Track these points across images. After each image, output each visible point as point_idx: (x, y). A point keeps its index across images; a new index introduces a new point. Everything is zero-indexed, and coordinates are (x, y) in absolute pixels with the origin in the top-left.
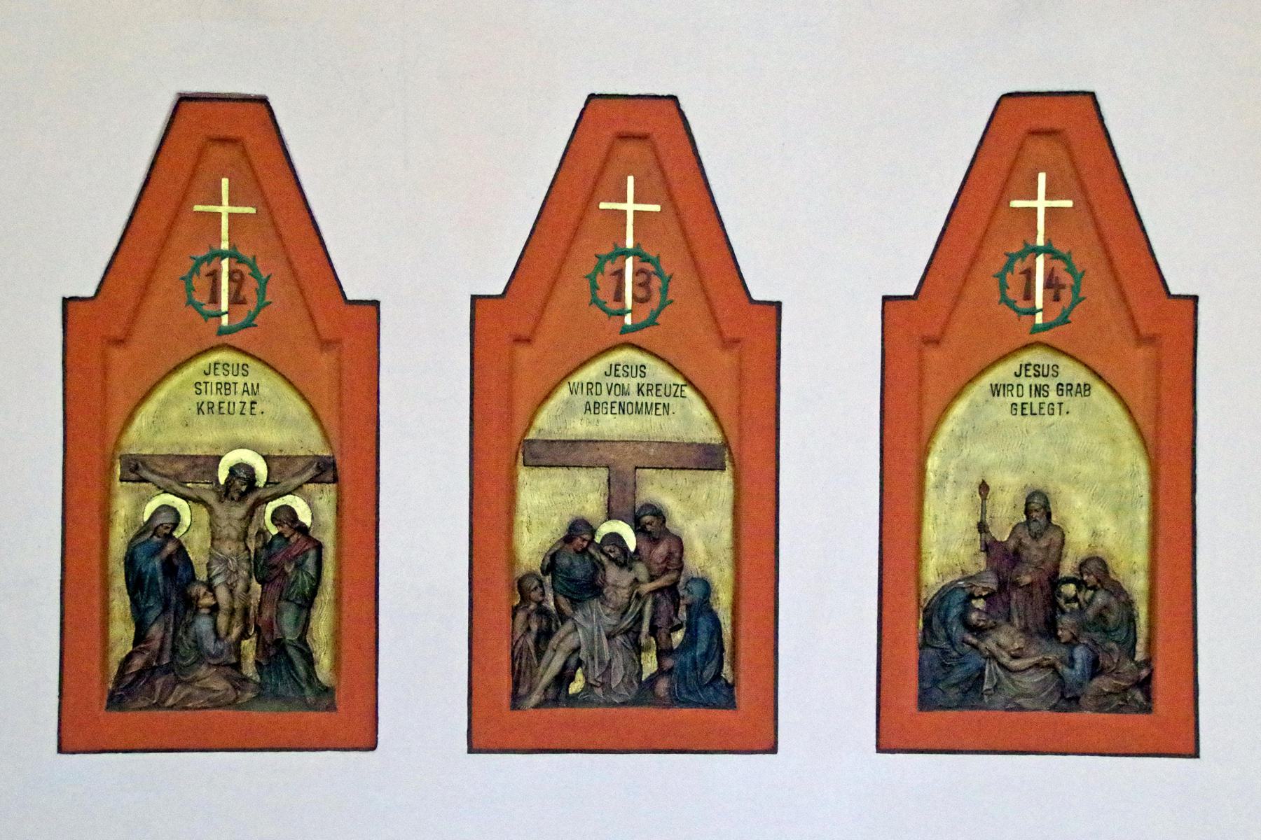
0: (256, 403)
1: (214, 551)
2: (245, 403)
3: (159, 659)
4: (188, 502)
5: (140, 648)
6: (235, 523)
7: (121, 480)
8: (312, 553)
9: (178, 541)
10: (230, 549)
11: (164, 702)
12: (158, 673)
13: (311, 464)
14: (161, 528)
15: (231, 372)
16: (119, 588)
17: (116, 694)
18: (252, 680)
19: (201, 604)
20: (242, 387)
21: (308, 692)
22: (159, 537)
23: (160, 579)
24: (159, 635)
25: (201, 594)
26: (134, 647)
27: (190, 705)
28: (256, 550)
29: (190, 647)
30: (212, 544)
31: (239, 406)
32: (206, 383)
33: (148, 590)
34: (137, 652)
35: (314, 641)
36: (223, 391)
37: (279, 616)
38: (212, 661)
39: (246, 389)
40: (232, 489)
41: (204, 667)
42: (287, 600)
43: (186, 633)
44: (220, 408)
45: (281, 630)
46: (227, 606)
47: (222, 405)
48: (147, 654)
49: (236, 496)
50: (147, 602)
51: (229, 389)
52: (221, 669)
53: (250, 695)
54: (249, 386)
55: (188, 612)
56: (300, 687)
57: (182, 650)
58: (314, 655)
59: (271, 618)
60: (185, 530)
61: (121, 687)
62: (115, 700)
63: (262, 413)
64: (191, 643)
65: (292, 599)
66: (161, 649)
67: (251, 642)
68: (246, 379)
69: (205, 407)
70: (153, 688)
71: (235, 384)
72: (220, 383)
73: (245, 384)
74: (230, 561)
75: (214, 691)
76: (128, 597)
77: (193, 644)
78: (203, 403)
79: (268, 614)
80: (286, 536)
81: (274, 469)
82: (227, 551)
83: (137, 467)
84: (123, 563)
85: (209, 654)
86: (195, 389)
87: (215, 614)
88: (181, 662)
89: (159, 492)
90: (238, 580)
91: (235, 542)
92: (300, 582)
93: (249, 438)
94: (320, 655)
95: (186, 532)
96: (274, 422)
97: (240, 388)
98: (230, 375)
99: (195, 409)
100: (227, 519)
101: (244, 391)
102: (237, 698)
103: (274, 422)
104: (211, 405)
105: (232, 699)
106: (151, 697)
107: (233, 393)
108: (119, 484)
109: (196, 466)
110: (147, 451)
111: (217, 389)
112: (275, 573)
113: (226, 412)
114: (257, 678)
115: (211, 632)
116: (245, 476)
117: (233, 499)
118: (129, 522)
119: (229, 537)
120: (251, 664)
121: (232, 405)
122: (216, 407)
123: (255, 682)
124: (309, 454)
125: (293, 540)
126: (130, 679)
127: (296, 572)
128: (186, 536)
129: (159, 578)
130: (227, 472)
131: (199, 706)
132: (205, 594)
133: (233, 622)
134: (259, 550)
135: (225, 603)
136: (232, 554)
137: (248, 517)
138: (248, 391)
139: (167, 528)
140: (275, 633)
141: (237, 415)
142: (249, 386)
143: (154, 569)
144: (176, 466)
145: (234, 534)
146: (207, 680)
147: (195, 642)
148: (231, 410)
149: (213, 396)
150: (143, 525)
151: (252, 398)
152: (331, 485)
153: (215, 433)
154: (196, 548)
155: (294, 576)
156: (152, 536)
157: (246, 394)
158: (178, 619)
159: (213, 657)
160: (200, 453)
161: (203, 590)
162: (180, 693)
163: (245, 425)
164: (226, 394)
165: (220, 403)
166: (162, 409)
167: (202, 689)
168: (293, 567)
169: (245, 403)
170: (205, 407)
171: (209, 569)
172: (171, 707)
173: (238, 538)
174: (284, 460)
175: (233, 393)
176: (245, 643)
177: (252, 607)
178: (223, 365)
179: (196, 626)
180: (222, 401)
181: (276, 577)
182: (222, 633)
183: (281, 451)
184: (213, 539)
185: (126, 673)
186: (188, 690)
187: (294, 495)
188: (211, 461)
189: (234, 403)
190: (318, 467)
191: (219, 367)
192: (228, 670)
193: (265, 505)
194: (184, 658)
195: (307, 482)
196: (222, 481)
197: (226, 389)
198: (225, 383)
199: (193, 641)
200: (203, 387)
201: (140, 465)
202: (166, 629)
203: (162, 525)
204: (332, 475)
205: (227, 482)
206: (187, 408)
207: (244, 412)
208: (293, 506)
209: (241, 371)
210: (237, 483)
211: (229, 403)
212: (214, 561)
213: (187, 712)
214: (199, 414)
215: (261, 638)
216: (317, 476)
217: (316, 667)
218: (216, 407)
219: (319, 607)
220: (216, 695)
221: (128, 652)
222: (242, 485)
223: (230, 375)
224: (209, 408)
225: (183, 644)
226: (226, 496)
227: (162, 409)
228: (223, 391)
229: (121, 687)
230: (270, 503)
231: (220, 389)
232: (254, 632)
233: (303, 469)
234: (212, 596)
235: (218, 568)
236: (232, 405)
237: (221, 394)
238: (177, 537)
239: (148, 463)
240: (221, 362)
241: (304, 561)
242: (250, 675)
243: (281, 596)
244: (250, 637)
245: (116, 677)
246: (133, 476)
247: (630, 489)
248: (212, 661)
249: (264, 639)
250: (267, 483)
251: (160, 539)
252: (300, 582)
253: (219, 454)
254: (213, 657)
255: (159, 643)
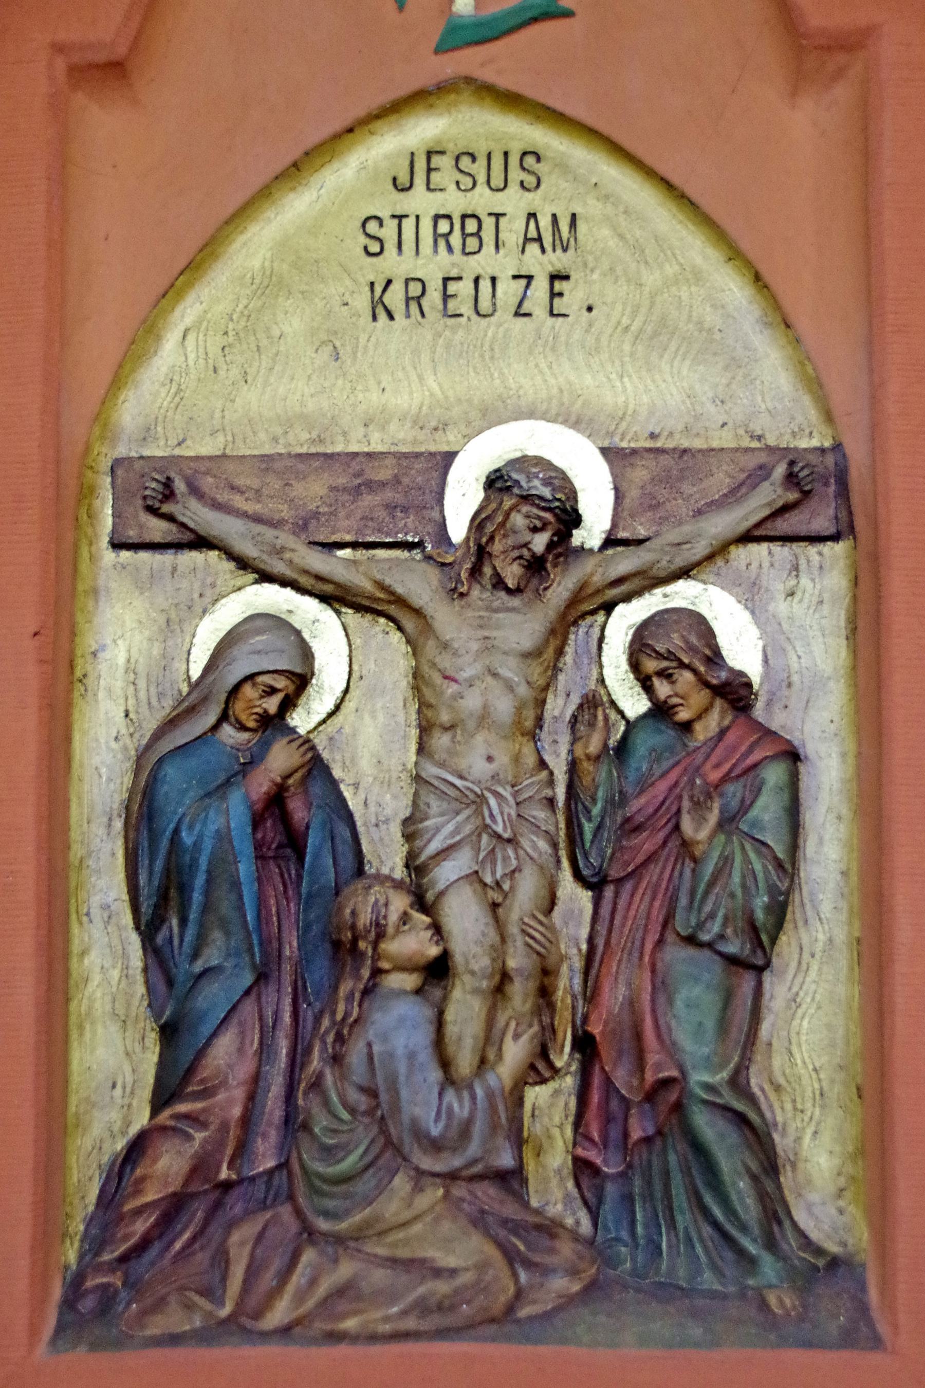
0: (567, 278)
1: (431, 770)
2: (530, 278)
3: (242, 1149)
4: (338, 613)
5: (178, 1117)
6: (510, 669)
7: (117, 545)
8: (774, 774)
9: (307, 742)
10: (490, 759)
11: (258, 1315)
12: (235, 1205)
13: (762, 473)
14: (248, 691)
15: (481, 178)
16: (105, 907)
17: (89, 1284)
18: (563, 1227)
19: (389, 958)
20: (520, 224)
21: (769, 1267)
22: (243, 728)
23: (245, 869)
24: (244, 1070)
25: (393, 917)
26: (155, 1112)
27: (350, 1324)
28: (573, 767)
29: (352, 1111)
30: (421, 749)
31: (509, 290)
32: (400, 218)
33: (206, 908)
34: (163, 1129)
35: (778, 1088)
36: (456, 240)
37: (661, 999)
38: (427, 1163)
39: (532, 233)
40: (497, 547)
41: (401, 1183)
42: (691, 940)
43: (337, 1060)
44: (446, 297)
45: (670, 1049)
46: (482, 963)
47: (452, 287)
48: (199, 1136)
49: (512, 573)
50: (195, 955)
51: (477, 235)
52: (459, 1190)
53: (560, 1284)
54: (545, 222)
55: (345, 988)
56: (741, 1252)
57: (321, 1122)
58: (776, 1137)
59: (632, 1003)
60: (329, 706)
61: (106, 1257)
62: (87, 1304)
63: (590, 309)
64: (354, 1096)
65: (705, 937)
66: (247, 1121)
67: (557, 1093)
68: (533, 200)
69: (395, 298)
70: (222, 1260)
71: (498, 216)
72: (448, 217)
73: (532, 216)
74: (493, 802)
75: (438, 1273)
76: (135, 940)
77: (362, 1102)
78: (389, 282)
79: (622, 991)
80: (683, 715)
81: (633, 494)
82: (479, 767)
83: (168, 493)
84: (119, 824)
85: (419, 1134)
86: (363, 240)
87: (438, 993)
88: (318, 1167)
89: (239, 582)
90: (518, 869)
91: (505, 738)
92: (736, 878)
93: (543, 394)
94: (798, 1140)
95: (331, 715)
96: (629, 337)
97: (513, 231)
98: (482, 188)
99: (362, 302)
100: (479, 653)
101: (527, 240)
102: (519, 1294)
103: (629, 337)
104: (415, 289)
105: (503, 1299)
106: (211, 1293)
107: (489, 246)
108: (109, 556)
109: (371, 486)
110: (207, 447)
111: (436, 236)
112: (646, 843)
113: (466, 309)
114: (578, 1223)
115: (426, 1056)
116: (546, 492)
117: (499, 583)
118: (142, 684)
119: (484, 718)
120: (559, 1171)
121: (485, 285)
122: (434, 296)
123: (575, 1236)
124: (747, 443)
125: (705, 730)
126: (140, 1227)
127: (722, 838)
128: (330, 727)
129: (242, 867)
130: (477, 496)
131: (387, 1328)
132: (405, 918)
133: (501, 1020)
134: (586, 765)
135: (478, 950)
136: (495, 777)
137: (550, 652)
138: (539, 239)
139: (272, 691)
140: (652, 1058)
141: (505, 315)
142: (545, 222)
143: (223, 837)
144: (298, 489)
145: (504, 707)
146: (417, 1228)
147: (372, 1093)
148: (485, 304)
149: (420, 262)
150: (185, 689)
151: (556, 260)
152: (828, 548)
153: (431, 382)
154: (366, 765)
155: (716, 854)
156: (216, 727)
157: (533, 248)
158: (308, 1015)
159: (436, 1146)
160: (377, 446)
161: (399, 903)
162: (313, 1282)
163: (531, 353)
164: (465, 253)
165: (446, 280)
166: (255, 304)
167: (393, 1262)
168: (713, 818)
169: (530, 278)
170: (395, 298)
171: (409, 837)
172: (285, 1332)
173: (518, 723)
174: (665, 460)
175: (489, 246)
176: (536, 1095)
177: (564, 969)
178: (457, 159)
179: (371, 1035)
180: (454, 273)
181: (651, 859)
182: (465, 1062)
183: (653, 436)
184: (425, 729)
185: (128, 1207)
186: (346, 1270)
187: (705, 583)
188: (416, 475)
189: (494, 280)
190: (791, 478)
191: (444, 162)
192: (488, 1193)
193: (600, 617)
194: (328, 1153)
195: (747, 538)
196: (458, 530)
197: (465, 235)
198: (464, 217)
199: (362, 1089)
200: (389, 232)
201: (180, 486)
202: (265, 1050)
203: (251, 677)
204: (831, 512)
205: (478, 523)
206: (336, 302)
207: (526, 307)
208: (703, 609)
209: (516, 174)
210: (518, 520)
211: (477, 281)
212: (435, 805)
213: (343, 1350)
214: (375, 318)
215: (597, 1080)
216: (786, 509)
217: (786, 1179)
218: (434, 296)
219: (794, 964)
220: (442, 1287)
221: (134, 1130)
222: (535, 530)
223: (482, 188)
224: (408, 300)
225: (326, 1103)
226: (475, 572)
227: (255, 304)
228: (456, 240)
229: (106, 1257)
230: (620, 609)
231: (447, 236)
232: (571, 1054)
233: (733, 491)
234: (428, 928)
235: (450, 827)
236: (485, 285)
237: (450, 249)
238: (302, 731)
239: (207, 483)
240: (450, 147)
241: (745, 808)
242: (555, 1209)
243: (666, 923)
244: (555, 1071)
245: (90, 1222)
246: (157, 529)
247: (275, 945)
248: (427, 1163)
249: (608, 1081)
250: (610, 542)
251: (246, 736)
252: (736, 878)
253: (446, 448)
254: (436, 1146)
255: (239, 1094)
